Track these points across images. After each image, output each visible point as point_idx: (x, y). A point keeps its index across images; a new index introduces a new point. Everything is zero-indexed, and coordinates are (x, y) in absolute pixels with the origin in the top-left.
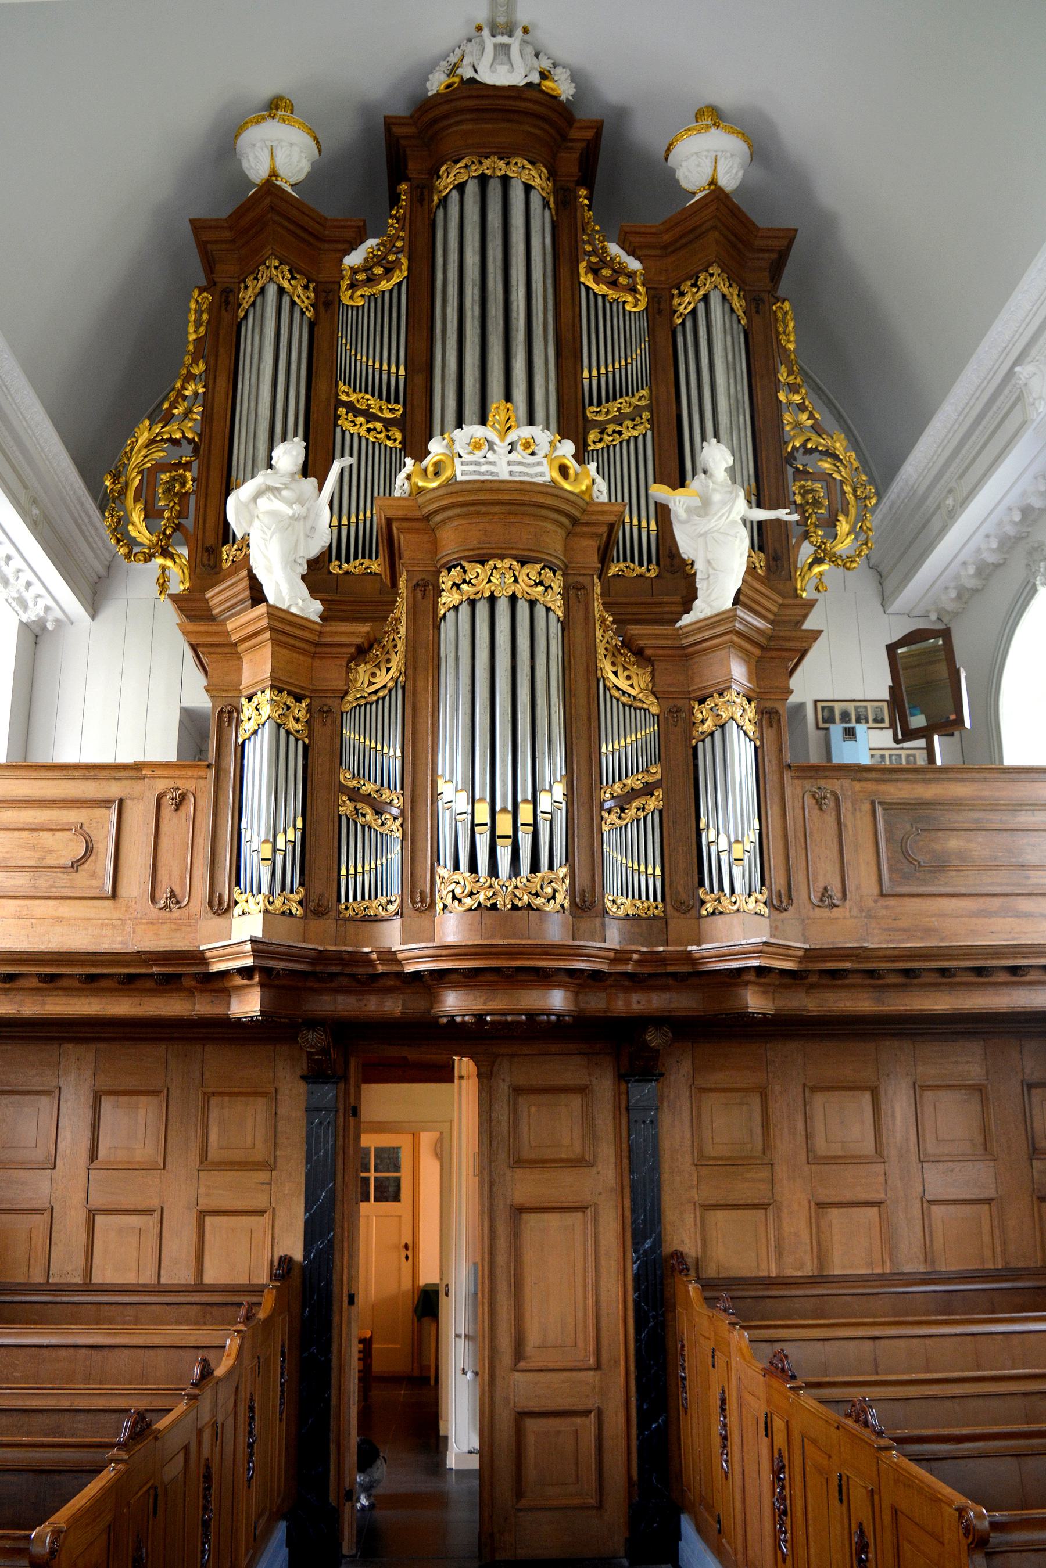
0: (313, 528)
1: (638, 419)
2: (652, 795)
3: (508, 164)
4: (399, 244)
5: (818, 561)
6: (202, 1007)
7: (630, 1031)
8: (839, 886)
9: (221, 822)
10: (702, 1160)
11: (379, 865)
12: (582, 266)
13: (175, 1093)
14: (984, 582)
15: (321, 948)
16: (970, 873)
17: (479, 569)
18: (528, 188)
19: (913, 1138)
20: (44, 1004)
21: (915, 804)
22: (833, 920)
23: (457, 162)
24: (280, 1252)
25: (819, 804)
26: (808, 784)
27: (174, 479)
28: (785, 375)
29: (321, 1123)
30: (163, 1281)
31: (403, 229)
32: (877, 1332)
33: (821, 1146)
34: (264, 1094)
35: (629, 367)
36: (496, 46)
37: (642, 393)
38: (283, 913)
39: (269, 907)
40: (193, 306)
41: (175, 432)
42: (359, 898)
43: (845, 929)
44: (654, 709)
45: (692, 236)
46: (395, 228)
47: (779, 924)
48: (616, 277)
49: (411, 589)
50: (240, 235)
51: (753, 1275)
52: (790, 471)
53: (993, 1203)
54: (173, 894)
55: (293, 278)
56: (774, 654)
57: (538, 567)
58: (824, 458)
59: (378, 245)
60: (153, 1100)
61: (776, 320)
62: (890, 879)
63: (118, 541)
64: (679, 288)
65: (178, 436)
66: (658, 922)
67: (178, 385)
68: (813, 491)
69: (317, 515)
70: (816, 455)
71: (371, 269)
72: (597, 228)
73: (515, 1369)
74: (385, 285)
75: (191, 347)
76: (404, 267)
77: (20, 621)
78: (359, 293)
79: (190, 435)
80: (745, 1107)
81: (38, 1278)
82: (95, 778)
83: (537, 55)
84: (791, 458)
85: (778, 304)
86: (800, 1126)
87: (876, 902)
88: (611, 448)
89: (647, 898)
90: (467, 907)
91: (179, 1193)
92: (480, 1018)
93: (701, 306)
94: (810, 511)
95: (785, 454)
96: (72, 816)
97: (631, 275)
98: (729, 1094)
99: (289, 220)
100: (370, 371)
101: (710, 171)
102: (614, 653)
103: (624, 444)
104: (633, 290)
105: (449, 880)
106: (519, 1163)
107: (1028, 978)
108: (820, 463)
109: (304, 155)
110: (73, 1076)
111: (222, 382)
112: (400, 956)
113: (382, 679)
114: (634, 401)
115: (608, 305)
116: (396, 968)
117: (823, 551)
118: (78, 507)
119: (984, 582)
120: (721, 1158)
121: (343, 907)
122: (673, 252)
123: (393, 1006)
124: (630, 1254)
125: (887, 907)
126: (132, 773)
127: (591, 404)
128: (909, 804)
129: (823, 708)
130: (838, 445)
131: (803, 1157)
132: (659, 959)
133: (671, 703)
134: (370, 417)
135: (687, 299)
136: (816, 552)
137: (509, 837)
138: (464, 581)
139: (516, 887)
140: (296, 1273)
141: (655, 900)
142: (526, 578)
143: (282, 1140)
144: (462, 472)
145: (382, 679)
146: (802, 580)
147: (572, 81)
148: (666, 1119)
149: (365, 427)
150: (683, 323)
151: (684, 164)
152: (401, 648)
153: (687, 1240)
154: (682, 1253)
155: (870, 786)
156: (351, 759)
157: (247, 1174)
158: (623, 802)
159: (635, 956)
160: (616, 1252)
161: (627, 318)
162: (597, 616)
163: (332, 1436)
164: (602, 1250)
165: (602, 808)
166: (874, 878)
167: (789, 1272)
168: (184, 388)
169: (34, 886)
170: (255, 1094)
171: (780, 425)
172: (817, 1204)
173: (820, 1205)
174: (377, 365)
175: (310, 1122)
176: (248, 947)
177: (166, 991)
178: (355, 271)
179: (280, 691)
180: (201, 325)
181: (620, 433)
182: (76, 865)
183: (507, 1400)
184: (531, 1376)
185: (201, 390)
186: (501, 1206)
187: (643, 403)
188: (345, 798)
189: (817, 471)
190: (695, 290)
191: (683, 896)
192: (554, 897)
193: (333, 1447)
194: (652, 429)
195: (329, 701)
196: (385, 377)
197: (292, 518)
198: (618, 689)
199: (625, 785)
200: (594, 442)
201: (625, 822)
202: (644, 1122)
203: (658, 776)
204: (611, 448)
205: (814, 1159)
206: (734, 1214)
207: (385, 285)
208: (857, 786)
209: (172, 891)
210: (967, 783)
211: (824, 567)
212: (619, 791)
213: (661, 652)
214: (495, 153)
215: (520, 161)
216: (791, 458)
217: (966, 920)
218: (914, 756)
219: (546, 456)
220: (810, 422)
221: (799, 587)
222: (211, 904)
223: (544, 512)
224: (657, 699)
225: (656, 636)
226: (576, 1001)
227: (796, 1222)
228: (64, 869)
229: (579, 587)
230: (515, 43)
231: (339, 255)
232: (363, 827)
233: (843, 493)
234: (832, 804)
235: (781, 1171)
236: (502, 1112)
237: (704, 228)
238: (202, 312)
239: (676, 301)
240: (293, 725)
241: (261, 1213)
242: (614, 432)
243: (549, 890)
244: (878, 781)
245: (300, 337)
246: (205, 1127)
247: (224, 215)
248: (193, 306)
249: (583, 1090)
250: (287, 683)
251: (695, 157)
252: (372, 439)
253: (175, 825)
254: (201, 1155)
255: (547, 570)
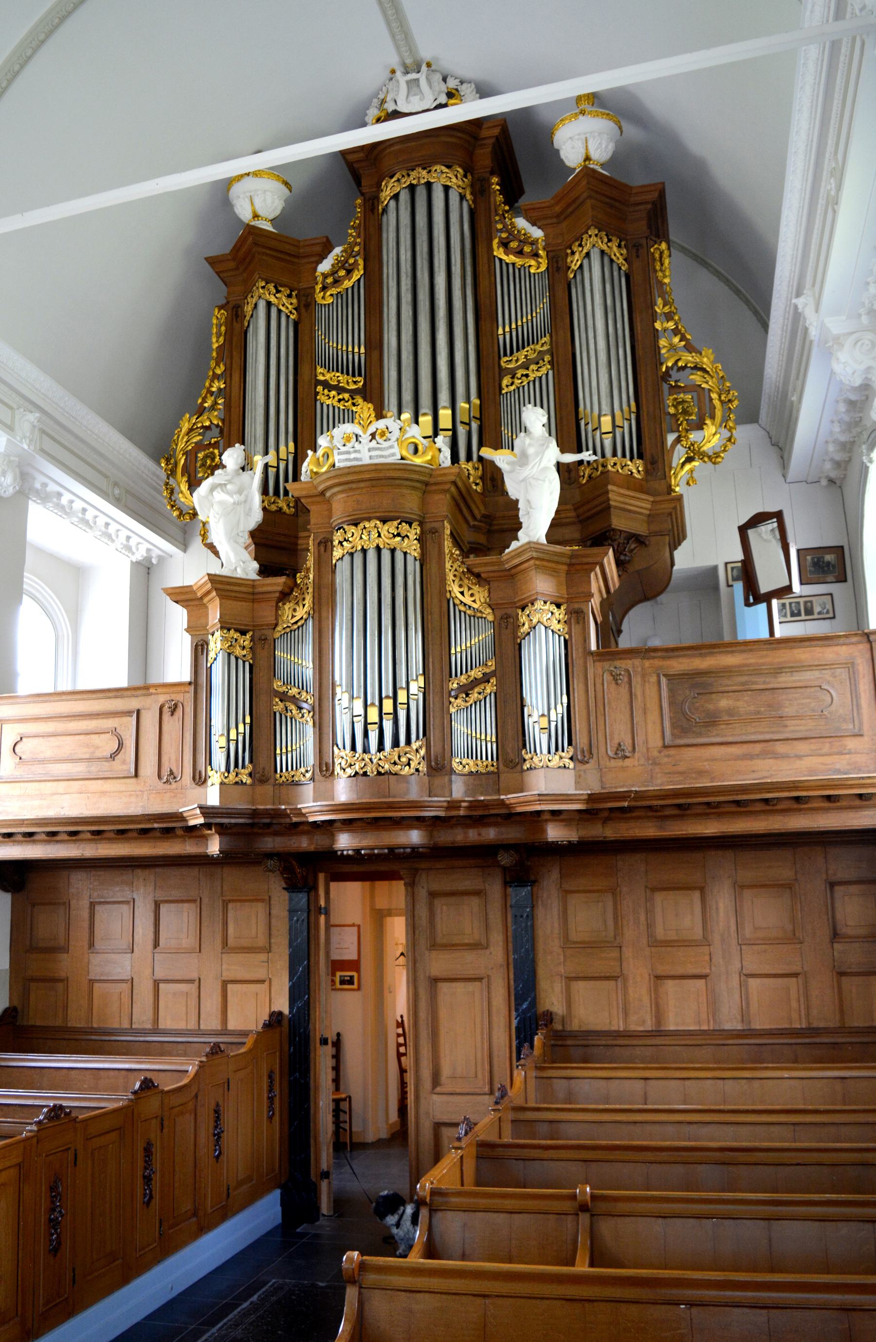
0: (250, 509)
1: (541, 362)
2: (489, 682)
3: (429, 172)
4: (356, 249)
5: (689, 460)
6: (189, 848)
7: (487, 852)
8: (630, 741)
9: (199, 721)
10: (567, 942)
11: (300, 742)
12: (495, 242)
13: (205, 900)
14: (848, 455)
15: (254, 808)
16: (737, 725)
17: (353, 529)
18: (447, 188)
19: (733, 928)
20: (97, 849)
21: (693, 674)
22: (624, 769)
23: (392, 177)
24: (275, 1008)
25: (615, 679)
26: (606, 665)
27: (206, 457)
28: (661, 307)
29: (298, 920)
30: (202, 1027)
31: (359, 236)
32: (647, 1074)
33: (660, 933)
34: (263, 901)
35: (534, 320)
36: (408, 82)
37: (544, 340)
38: (237, 783)
39: (225, 781)
40: (215, 321)
41: (205, 421)
42: (290, 769)
43: (633, 777)
44: (490, 618)
45: (574, 206)
46: (353, 236)
47: (582, 773)
48: (521, 245)
49: (316, 546)
50: (250, 261)
51: (606, 1029)
52: (665, 387)
53: (800, 977)
54: (171, 773)
55: (278, 291)
56: (578, 567)
57: (395, 523)
58: (694, 372)
59: (342, 252)
60: (192, 906)
61: (654, 260)
62: (672, 734)
63: (172, 506)
64: (571, 248)
65: (207, 423)
66: (492, 776)
67: (207, 384)
68: (684, 401)
69: (252, 500)
70: (688, 371)
71: (337, 272)
72: (507, 208)
73: (433, 1092)
74: (347, 284)
75: (214, 354)
76: (361, 267)
77: (132, 561)
78: (328, 293)
79: (215, 422)
80: (600, 904)
81: (126, 1025)
82: (122, 697)
83: (445, 80)
84: (667, 374)
85: (656, 246)
86: (642, 917)
87: (660, 752)
88: (521, 389)
89: (487, 759)
90: (348, 774)
91: (211, 968)
92: (357, 851)
93: (586, 262)
94: (681, 419)
95: (660, 374)
96: (110, 723)
97: (534, 243)
98: (588, 895)
99: (270, 249)
100: (340, 353)
101: (583, 151)
102: (460, 578)
103: (531, 384)
104: (536, 255)
105: (342, 755)
106: (434, 946)
107: (779, 807)
108: (692, 377)
109: (276, 197)
110: (142, 890)
111: (236, 377)
112: (304, 811)
113: (301, 612)
114: (538, 348)
115: (517, 271)
116: (303, 819)
117: (692, 452)
118: (155, 478)
119: (848, 455)
120: (581, 943)
121: (278, 776)
122: (565, 219)
123: (304, 844)
124: (514, 1014)
125: (668, 756)
126: (144, 692)
127: (505, 355)
128: (687, 674)
129: (732, 568)
130: (705, 360)
131: (644, 941)
132: (483, 805)
133: (503, 612)
134: (340, 390)
135: (577, 256)
136: (687, 453)
137: (376, 723)
138: (345, 540)
139: (380, 759)
140: (285, 1023)
141: (492, 759)
142: (387, 533)
143: (274, 932)
144: (340, 460)
145: (301, 612)
146: (675, 478)
147: (477, 92)
148: (540, 912)
149: (336, 399)
150: (575, 276)
151: (563, 147)
152: (310, 590)
153: (556, 1003)
154: (551, 1014)
155: (657, 663)
156: (281, 670)
157: (253, 955)
158: (466, 690)
159: (464, 804)
160: (504, 1010)
161: (532, 279)
162: (447, 551)
163: (312, 1134)
164: (494, 1009)
165: (450, 696)
166: (659, 734)
167: (633, 1027)
168: (211, 386)
169: (89, 772)
170: (257, 900)
171: (657, 349)
172: (656, 977)
173: (658, 977)
174: (344, 348)
175: (291, 919)
176: (198, 811)
177: (168, 838)
178: (325, 276)
179: (229, 630)
180: (221, 335)
181: (527, 376)
182: (113, 756)
183: (428, 1113)
184: (445, 1098)
185: (223, 386)
186: (422, 977)
187: (545, 348)
188: (277, 700)
189: (689, 383)
190: (580, 249)
191: (511, 756)
192: (409, 764)
193: (312, 1141)
194: (553, 368)
195: (265, 632)
196: (350, 356)
197: (234, 503)
198: (465, 605)
199: (469, 676)
200: (507, 386)
201: (468, 704)
202: (522, 916)
203: (493, 668)
204: (521, 389)
205: (655, 943)
206: (592, 983)
207: (347, 284)
208: (647, 663)
209: (171, 770)
210: (736, 654)
211: (696, 463)
212: (465, 681)
213: (492, 575)
214: (419, 165)
215: (439, 167)
216: (667, 374)
217: (732, 762)
218: (811, 602)
219: (397, 440)
220: (683, 343)
221: (673, 483)
222: (194, 778)
223: (397, 482)
224: (493, 610)
225: (486, 564)
226: (431, 836)
227: (639, 990)
228: (105, 759)
229: (434, 531)
230: (422, 77)
231: (314, 265)
232: (291, 719)
233: (711, 399)
234: (626, 679)
235: (628, 952)
236: (422, 912)
237: (581, 199)
238: (221, 325)
239: (569, 260)
240: (238, 651)
241: (262, 981)
242: (522, 375)
243: (404, 759)
244: (663, 658)
245: (287, 335)
246: (225, 924)
247: (228, 252)
248: (215, 321)
249: (478, 893)
250: (232, 623)
251: (570, 141)
252: (342, 407)
253: (172, 725)
254: (223, 943)
255: (404, 524)
